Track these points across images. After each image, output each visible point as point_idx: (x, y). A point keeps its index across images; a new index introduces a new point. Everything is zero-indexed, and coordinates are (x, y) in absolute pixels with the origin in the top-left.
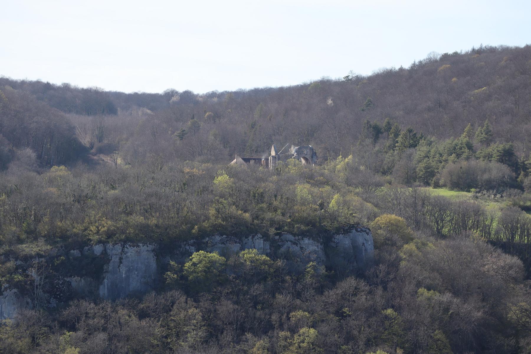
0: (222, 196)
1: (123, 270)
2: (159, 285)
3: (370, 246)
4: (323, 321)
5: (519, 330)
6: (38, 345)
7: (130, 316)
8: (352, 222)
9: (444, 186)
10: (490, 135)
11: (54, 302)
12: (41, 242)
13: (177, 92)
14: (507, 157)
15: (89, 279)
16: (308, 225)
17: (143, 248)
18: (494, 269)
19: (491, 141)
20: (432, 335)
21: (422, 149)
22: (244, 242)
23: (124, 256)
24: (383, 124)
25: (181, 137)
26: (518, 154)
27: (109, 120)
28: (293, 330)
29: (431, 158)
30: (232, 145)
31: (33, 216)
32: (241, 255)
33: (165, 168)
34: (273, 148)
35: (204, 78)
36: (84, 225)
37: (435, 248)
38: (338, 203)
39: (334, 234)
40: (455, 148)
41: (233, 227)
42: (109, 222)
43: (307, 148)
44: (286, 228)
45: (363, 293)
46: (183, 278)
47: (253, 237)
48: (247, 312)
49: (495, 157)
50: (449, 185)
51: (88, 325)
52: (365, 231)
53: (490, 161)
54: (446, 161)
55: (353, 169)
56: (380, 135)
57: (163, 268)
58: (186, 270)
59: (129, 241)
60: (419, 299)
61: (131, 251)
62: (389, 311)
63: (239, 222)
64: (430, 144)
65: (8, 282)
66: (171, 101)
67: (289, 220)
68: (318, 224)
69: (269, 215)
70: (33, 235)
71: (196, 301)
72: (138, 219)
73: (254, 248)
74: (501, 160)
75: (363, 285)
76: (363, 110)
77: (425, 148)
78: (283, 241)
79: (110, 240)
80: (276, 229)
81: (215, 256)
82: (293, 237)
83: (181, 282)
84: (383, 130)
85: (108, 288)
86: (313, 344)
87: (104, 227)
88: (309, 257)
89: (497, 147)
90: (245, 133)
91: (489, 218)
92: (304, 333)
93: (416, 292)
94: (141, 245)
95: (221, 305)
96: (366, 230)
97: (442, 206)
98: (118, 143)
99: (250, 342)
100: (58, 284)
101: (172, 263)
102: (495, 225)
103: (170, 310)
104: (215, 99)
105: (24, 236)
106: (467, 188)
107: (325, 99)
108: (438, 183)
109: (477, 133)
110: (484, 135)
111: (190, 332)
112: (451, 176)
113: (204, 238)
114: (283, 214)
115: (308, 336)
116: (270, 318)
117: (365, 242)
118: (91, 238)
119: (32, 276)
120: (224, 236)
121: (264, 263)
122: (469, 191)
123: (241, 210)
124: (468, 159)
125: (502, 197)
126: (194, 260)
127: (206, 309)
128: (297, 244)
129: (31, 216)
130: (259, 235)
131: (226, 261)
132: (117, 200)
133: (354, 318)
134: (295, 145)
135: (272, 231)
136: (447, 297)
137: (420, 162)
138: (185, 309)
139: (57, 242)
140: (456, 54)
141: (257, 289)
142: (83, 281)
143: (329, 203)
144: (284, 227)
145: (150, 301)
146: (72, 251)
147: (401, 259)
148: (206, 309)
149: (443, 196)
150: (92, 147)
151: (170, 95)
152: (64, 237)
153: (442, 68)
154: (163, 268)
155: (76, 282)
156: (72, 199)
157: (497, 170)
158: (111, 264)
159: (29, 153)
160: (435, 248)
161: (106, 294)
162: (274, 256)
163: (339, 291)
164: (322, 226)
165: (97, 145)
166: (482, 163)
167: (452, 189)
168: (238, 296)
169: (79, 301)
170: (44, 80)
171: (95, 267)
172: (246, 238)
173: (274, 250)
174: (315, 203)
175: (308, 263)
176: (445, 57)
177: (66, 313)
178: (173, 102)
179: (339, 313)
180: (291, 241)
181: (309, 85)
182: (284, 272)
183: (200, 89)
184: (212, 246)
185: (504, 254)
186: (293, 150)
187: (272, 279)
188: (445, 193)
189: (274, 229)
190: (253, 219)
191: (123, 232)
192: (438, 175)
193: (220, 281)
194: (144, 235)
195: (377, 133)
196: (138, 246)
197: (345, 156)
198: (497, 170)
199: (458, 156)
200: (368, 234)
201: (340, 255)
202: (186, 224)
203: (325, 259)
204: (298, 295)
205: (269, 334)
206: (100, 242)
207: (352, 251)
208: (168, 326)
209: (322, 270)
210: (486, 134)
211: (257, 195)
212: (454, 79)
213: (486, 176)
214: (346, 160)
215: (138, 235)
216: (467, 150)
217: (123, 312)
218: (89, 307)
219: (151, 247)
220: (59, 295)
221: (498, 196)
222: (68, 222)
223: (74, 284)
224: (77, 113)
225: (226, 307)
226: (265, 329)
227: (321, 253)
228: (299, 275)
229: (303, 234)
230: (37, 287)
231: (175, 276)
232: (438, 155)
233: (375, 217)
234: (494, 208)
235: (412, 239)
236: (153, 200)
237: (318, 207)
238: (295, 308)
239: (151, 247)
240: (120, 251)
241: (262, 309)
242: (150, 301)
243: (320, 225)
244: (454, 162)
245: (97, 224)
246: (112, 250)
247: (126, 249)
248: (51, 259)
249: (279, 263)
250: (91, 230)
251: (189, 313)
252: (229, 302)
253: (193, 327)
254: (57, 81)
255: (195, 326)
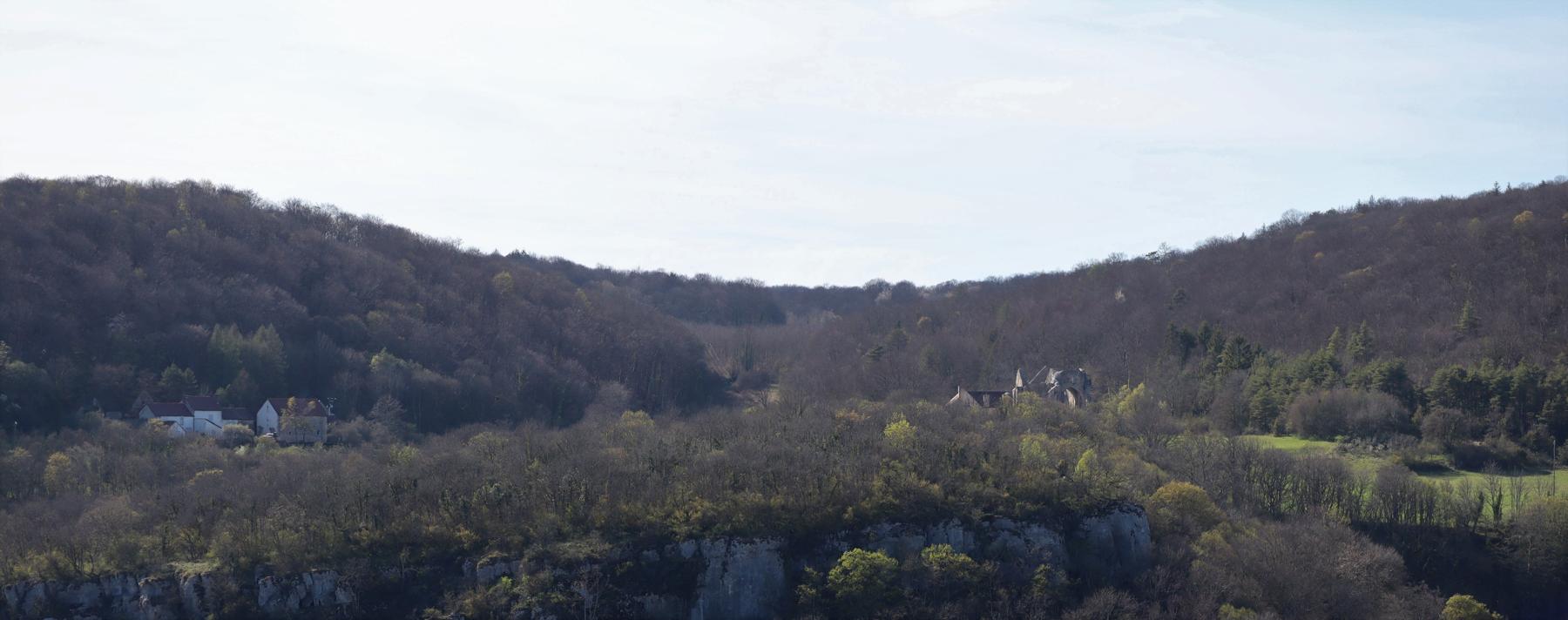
1: (729, 582)
3: (1143, 535)
8: (1113, 496)
9: (1293, 432)
12: (595, 537)
13: (887, 285)
14: (1395, 381)
16: (1036, 502)
19: (1372, 355)
21: (1260, 370)
25: (877, 357)
26: (1413, 376)
27: (765, 333)
30: (953, 369)
37: (1257, 536)
38: (1089, 464)
42: (706, 504)
44: (1001, 508)
46: (829, 594)
47: (946, 524)
54: (1296, 390)
55: (1141, 406)
57: (795, 578)
59: (733, 535)
61: (742, 551)
65: (541, 604)
69: (973, 487)
70: (582, 526)
72: (753, 497)
74: (1385, 388)
75: (1127, 600)
77: (1262, 370)
79: (707, 533)
80: (985, 510)
81: (880, 556)
89: (1377, 367)
93: (1216, 611)
96: (1138, 510)
97: (1279, 465)
102: (1367, 495)
104: (949, 295)
105: (567, 528)
114: (997, 485)
121: (963, 566)
122: (1333, 441)
124: (1331, 386)
130: (956, 521)
134: (1057, 368)
135: (977, 514)
139: (621, 538)
147: (1194, 557)
151: (877, 288)
152: (633, 529)
153: (1300, 237)
157: (1378, 404)
159: (617, 390)
160: (1257, 536)
162: (979, 555)
167: (1306, 437)
170: (668, 271)
173: (981, 543)
174: (1052, 465)
183: (926, 278)
190: (946, 495)
194: (763, 523)
195: (1187, 345)
196: (752, 542)
197: (1134, 385)
198: (1378, 404)
199: (1317, 382)
206: (690, 536)
209: (1062, 577)
212: (1318, 255)
213: (1360, 415)
216: (1331, 372)
219: (774, 544)
221: (1380, 447)
229: (1030, 518)
232: (1283, 381)
234: (1367, 467)
235: (1217, 522)
239: (774, 544)
244: (1308, 392)
245: (686, 506)
249: (988, 567)
254: (689, 272)
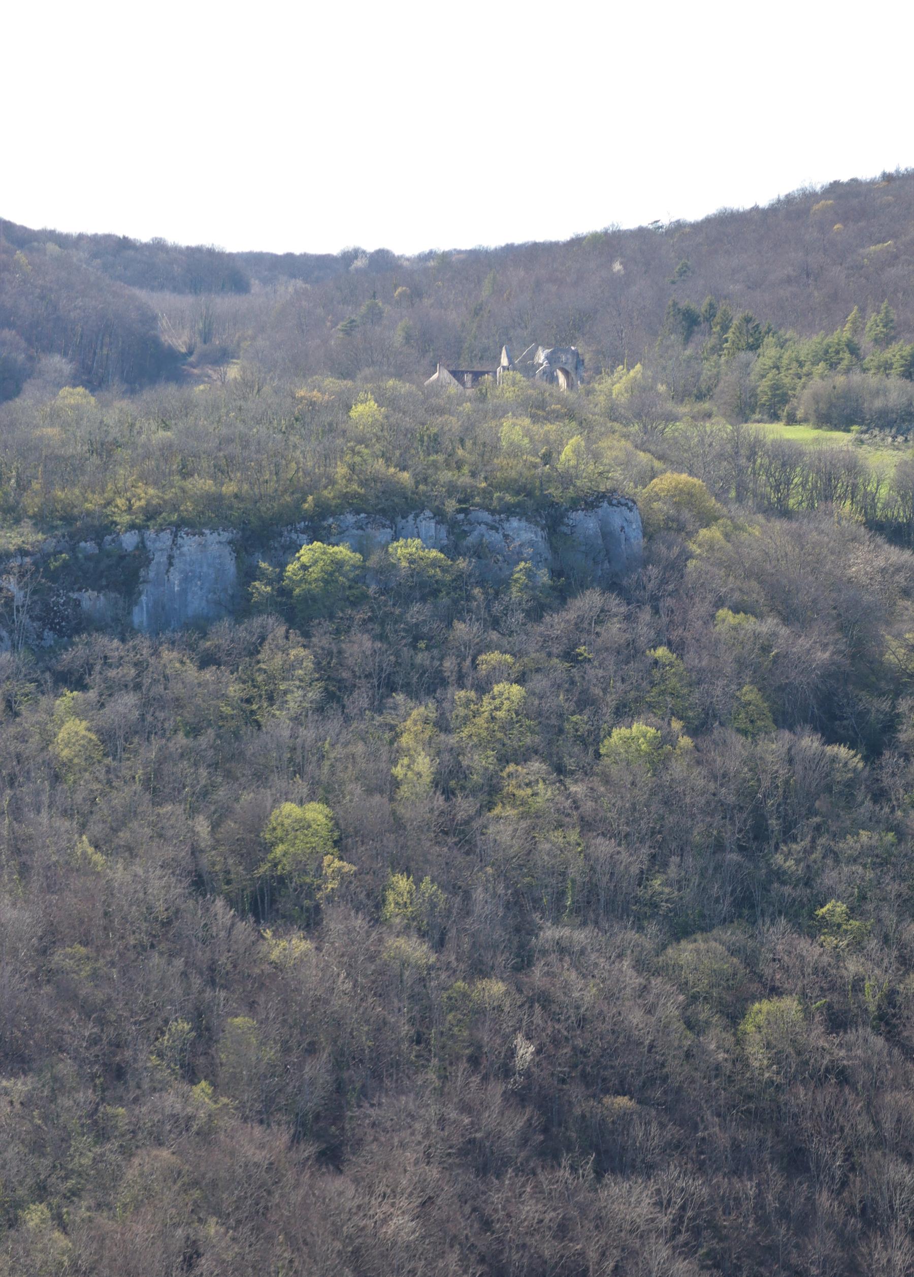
0: (361, 441)
1: (175, 577)
2: (241, 607)
3: (635, 533)
4: (538, 670)
5: (900, 684)
6: (17, 714)
7: (182, 663)
8: (602, 488)
9: (805, 420)
10: (892, 328)
11: (49, 637)
12: (27, 526)
13: (364, 252)
15: (113, 595)
17: (212, 538)
18: (866, 573)
20: (738, 693)
21: (769, 352)
22: (400, 526)
23: (176, 553)
24: (701, 308)
27: (225, 303)
28: (482, 688)
29: (782, 370)
30: (430, 345)
31: (13, 481)
32: (390, 550)
33: (266, 389)
34: (504, 351)
35: (418, 224)
36: (106, 495)
37: (761, 534)
38: (576, 452)
39: (567, 510)
40: (826, 352)
41: (378, 497)
42: (151, 491)
43: (567, 351)
44: (477, 500)
45: (615, 619)
46: (285, 592)
47: (417, 516)
48: (397, 654)
49: (897, 369)
50: (813, 419)
51: (106, 680)
52: (626, 505)
53: (887, 375)
54: (809, 374)
55: (640, 390)
56: (696, 328)
57: (249, 574)
58: (290, 578)
60: (717, 628)
61: (189, 544)
62: (661, 652)
63: (390, 490)
64: (782, 345)
66: (352, 267)
67: (484, 485)
68: (537, 493)
69: (446, 476)
71: (307, 635)
72: (202, 484)
73: (419, 537)
75: (616, 605)
76: (673, 283)
78: (471, 524)
80: (460, 501)
81: (342, 551)
82: (490, 517)
83: (279, 599)
84: (701, 319)
85: (148, 611)
86: (517, 714)
87: (140, 499)
88: (520, 553)
90: (463, 325)
91: (874, 477)
92: (501, 694)
93: (713, 617)
94: (207, 531)
95: (350, 641)
96: (629, 503)
97: (786, 458)
98: (238, 345)
99: (402, 711)
100: (57, 604)
101: (263, 565)
102: (883, 492)
103: (258, 652)
104: (431, 263)
106: (844, 424)
107: (611, 260)
108: (794, 415)
109: (869, 325)
110: (880, 329)
111: (293, 692)
112: (817, 403)
113: (324, 519)
114: (473, 474)
115: (508, 699)
116: (441, 665)
117: (625, 524)
118: (117, 519)
119: (9, 590)
120: (362, 515)
121: (434, 563)
122: (849, 431)
123: (395, 467)
124: (848, 371)
125: (906, 440)
126: (303, 559)
127: (323, 649)
128: (497, 530)
129: (9, 479)
130: (428, 513)
131: (364, 561)
132: (167, 450)
133: (596, 663)
134: (546, 345)
135: (451, 505)
136: (769, 625)
137: (763, 376)
138: (285, 651)
139: (56, 528)
140: (854, 181)
141: (417, 612)
142: (102, 597)
143: (560, 453)
144: (473, 497)
145: (223, 635)
146: (82, 544)
147: (690, 556)
148: (323, 649)
149: (788, 440)
150: (190, 353)
151: (350, 257)
152: (68, 519)
154: (249, 574)
155: (91, 600)
156: (86, 448)
158: (153, 567)
160: (761, 534)
161: (145, 624)
162: (453, 551)
163: (571, 615)
164: (546, 496)
165: (200, 347)
166: (873, 380)
167: (818, 426)
168: (382, 624)
169: (90, 635)
171: (123, 574)
172: (403, 518)
175: (517, 563)
176: (835, 187)
177: (67, 656)
178: (357, 270)
179: (570, 656)
180: (486, 524)
181: (585, 238)
182: (472, 580)
183: (407, 245)
184: (340, 533)
185: (886, 546)
186: (541, 356)
187: (448, 594)
188: (801, 435)
189: (454, 502)
190: (417, 483)
191: (175, 508)
192: (794, 401)
193: (352, 598)
194: (214, 513)
195: (690, 322)
196: (202, 534)
197: (631, 366)
199: (833, 366)
200: (631, 510)
201: (583, 548)
202: (293, 493)
203: (550, 558)
204: (495, 623)
205: (437, 695)
206: (132, 526)
207: (600, 541)
208: (253, 681)
209: (544, 577)
210: (884, 326)
211: (426, 438)
213: (878, 403)
214: (632, 373)
215: (203, 513)
216: (847, 355)
217: (168, 655)
218: (112, 646)
219: (226, 536)
220: (59, 623)
221: (900, 439)
222: (77, 491)
223: (86, 604)
224: (175, 289)
225: (360, 646)
226: (431, 685)
227: (542, 545)
228: (502, 585)
229: (509, 511)
230: (18, 611)
231: (269, 589)
233: (652, 478)
235: (716, 519)
236: (235, 449)
237: (538, 460)
238: (489, 647)
239: (226, 536)
240: (169, 543)
241: (428, 648)
242: (223, 635)
243: (541, 494)
244: (822, 377)
245: (127, 495)
246: (155, 541)
247: (180, 541)
248: (42, 558)
249: (462, 564)
250: (117, 506)
251: (291, 657)
252: (366, 636)
253: (297, 683)
254: (142, 234)
255: (301, 680)
